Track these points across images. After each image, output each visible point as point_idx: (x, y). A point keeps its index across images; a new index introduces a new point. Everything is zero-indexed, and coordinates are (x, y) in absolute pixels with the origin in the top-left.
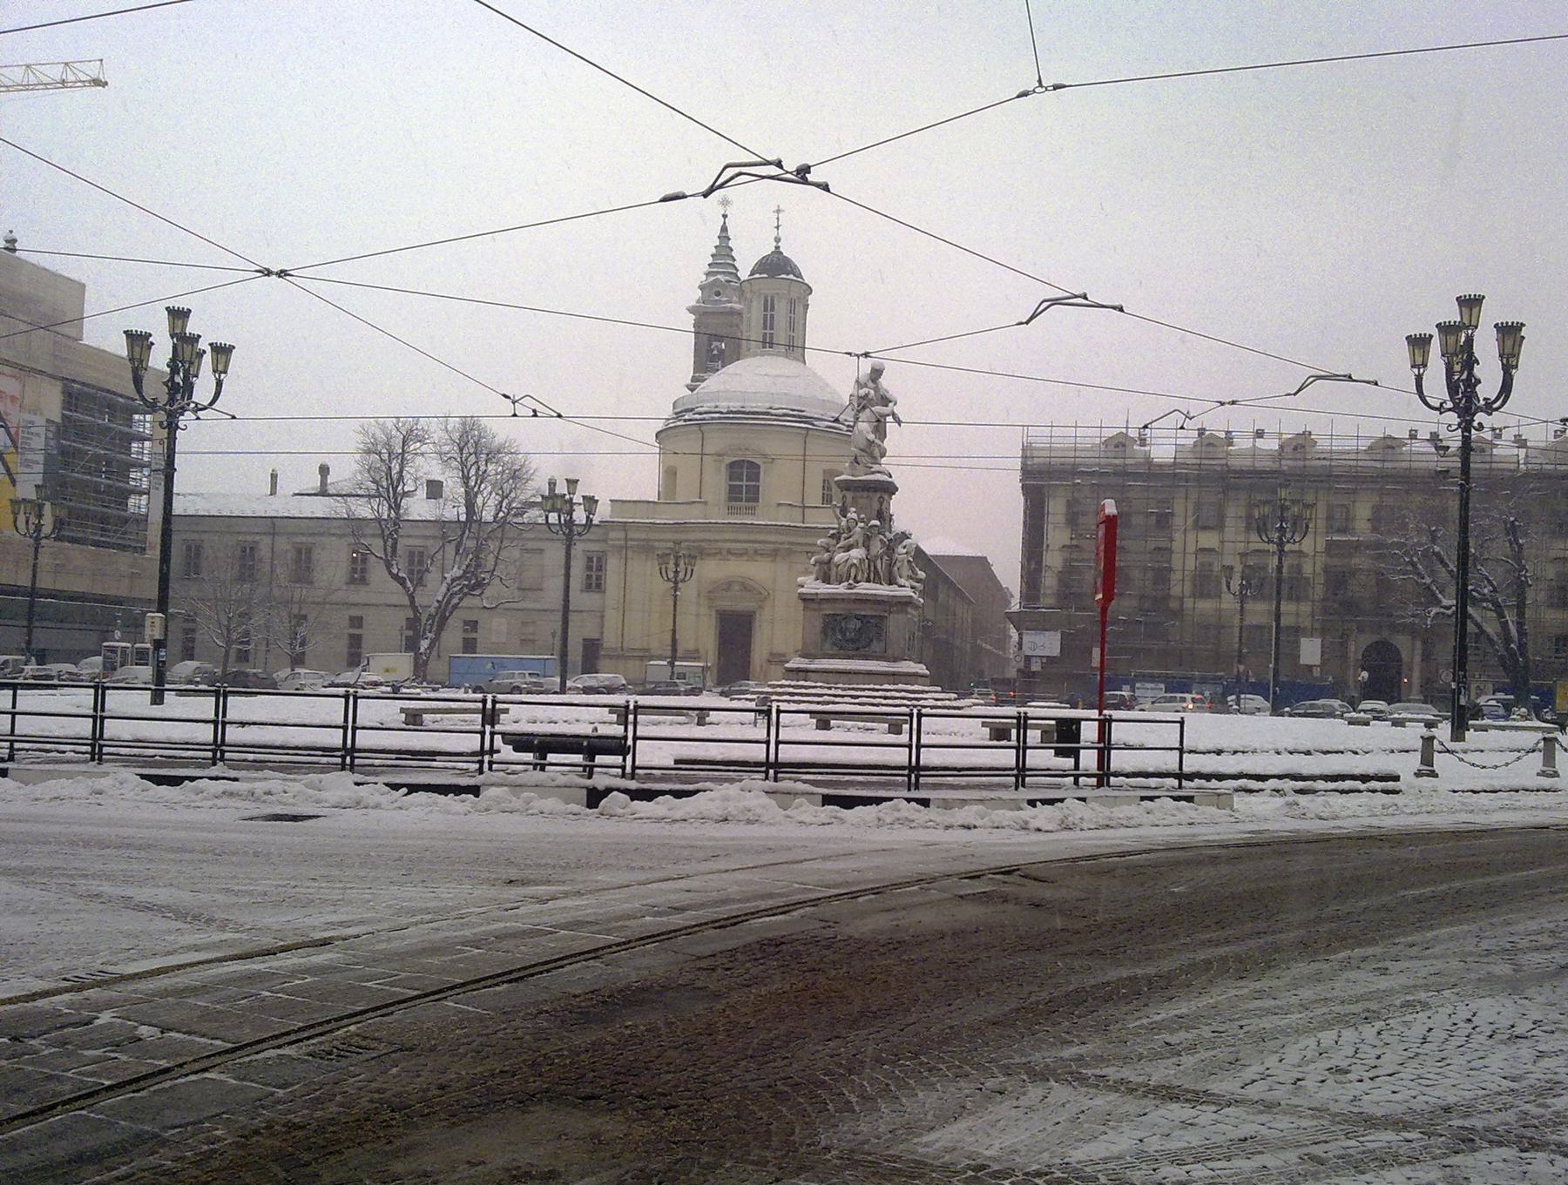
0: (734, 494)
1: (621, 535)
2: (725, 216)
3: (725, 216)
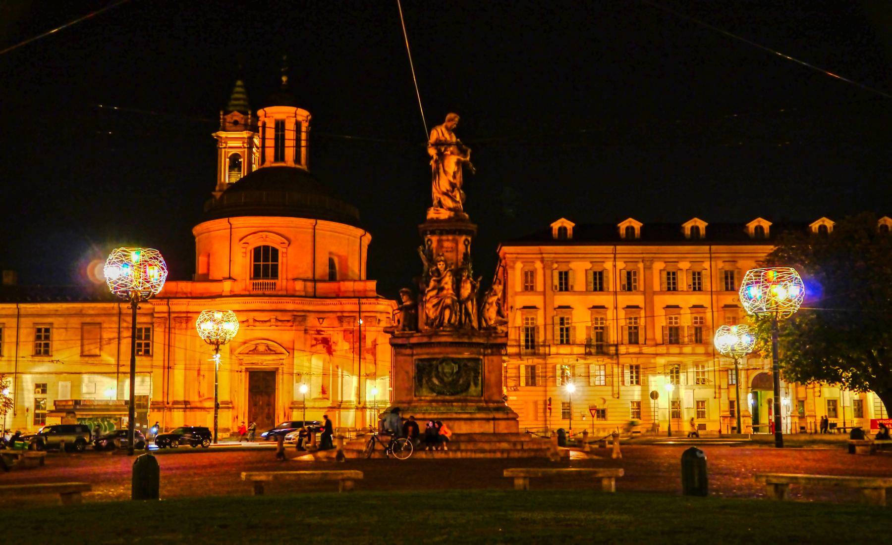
0: (257, 273)
1: (164, 308)
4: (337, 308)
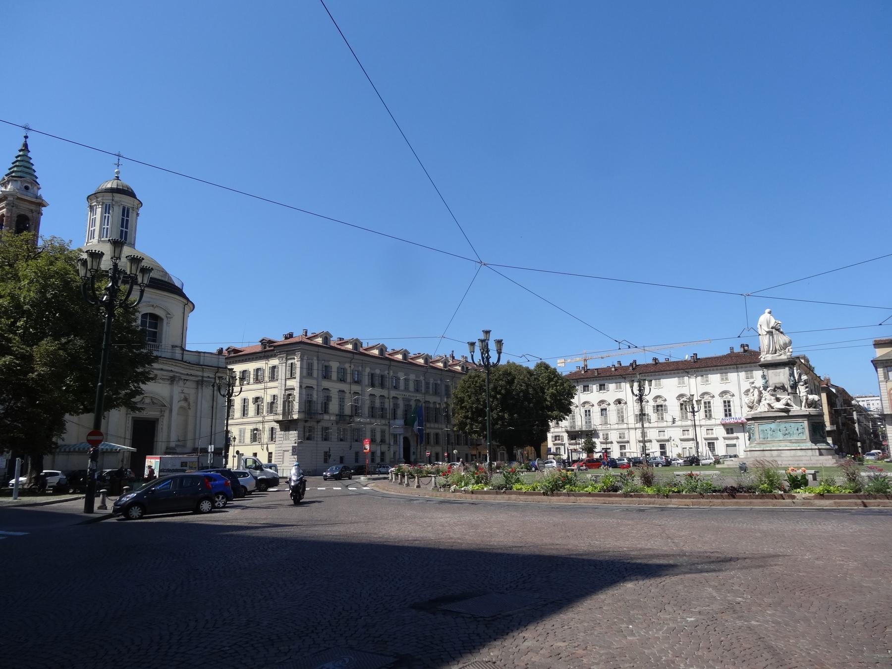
2: (26, 137)
3: (26, 137)
4: (200, 373)
